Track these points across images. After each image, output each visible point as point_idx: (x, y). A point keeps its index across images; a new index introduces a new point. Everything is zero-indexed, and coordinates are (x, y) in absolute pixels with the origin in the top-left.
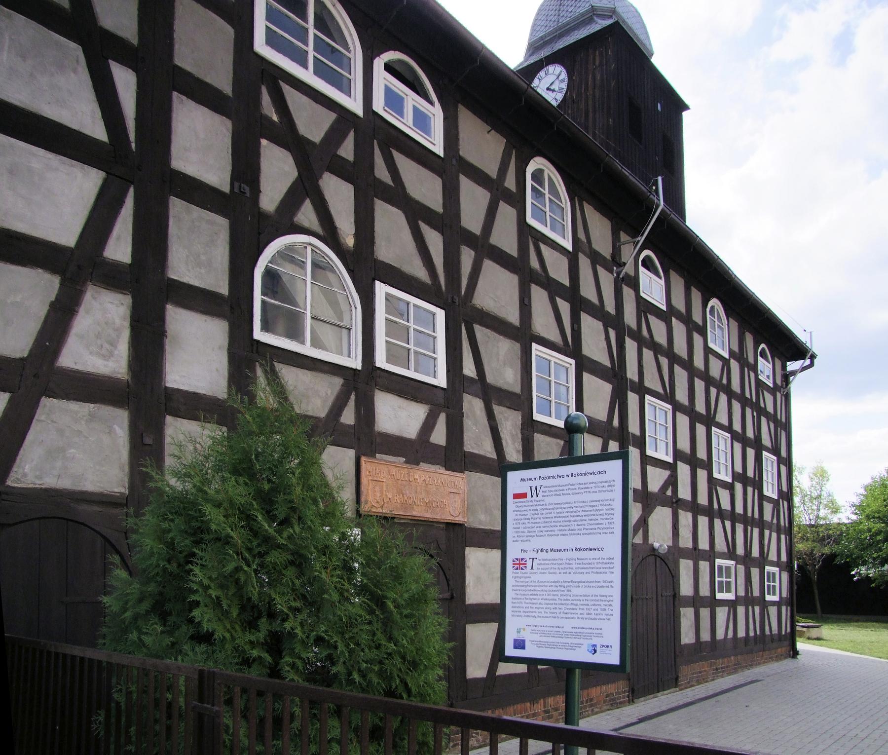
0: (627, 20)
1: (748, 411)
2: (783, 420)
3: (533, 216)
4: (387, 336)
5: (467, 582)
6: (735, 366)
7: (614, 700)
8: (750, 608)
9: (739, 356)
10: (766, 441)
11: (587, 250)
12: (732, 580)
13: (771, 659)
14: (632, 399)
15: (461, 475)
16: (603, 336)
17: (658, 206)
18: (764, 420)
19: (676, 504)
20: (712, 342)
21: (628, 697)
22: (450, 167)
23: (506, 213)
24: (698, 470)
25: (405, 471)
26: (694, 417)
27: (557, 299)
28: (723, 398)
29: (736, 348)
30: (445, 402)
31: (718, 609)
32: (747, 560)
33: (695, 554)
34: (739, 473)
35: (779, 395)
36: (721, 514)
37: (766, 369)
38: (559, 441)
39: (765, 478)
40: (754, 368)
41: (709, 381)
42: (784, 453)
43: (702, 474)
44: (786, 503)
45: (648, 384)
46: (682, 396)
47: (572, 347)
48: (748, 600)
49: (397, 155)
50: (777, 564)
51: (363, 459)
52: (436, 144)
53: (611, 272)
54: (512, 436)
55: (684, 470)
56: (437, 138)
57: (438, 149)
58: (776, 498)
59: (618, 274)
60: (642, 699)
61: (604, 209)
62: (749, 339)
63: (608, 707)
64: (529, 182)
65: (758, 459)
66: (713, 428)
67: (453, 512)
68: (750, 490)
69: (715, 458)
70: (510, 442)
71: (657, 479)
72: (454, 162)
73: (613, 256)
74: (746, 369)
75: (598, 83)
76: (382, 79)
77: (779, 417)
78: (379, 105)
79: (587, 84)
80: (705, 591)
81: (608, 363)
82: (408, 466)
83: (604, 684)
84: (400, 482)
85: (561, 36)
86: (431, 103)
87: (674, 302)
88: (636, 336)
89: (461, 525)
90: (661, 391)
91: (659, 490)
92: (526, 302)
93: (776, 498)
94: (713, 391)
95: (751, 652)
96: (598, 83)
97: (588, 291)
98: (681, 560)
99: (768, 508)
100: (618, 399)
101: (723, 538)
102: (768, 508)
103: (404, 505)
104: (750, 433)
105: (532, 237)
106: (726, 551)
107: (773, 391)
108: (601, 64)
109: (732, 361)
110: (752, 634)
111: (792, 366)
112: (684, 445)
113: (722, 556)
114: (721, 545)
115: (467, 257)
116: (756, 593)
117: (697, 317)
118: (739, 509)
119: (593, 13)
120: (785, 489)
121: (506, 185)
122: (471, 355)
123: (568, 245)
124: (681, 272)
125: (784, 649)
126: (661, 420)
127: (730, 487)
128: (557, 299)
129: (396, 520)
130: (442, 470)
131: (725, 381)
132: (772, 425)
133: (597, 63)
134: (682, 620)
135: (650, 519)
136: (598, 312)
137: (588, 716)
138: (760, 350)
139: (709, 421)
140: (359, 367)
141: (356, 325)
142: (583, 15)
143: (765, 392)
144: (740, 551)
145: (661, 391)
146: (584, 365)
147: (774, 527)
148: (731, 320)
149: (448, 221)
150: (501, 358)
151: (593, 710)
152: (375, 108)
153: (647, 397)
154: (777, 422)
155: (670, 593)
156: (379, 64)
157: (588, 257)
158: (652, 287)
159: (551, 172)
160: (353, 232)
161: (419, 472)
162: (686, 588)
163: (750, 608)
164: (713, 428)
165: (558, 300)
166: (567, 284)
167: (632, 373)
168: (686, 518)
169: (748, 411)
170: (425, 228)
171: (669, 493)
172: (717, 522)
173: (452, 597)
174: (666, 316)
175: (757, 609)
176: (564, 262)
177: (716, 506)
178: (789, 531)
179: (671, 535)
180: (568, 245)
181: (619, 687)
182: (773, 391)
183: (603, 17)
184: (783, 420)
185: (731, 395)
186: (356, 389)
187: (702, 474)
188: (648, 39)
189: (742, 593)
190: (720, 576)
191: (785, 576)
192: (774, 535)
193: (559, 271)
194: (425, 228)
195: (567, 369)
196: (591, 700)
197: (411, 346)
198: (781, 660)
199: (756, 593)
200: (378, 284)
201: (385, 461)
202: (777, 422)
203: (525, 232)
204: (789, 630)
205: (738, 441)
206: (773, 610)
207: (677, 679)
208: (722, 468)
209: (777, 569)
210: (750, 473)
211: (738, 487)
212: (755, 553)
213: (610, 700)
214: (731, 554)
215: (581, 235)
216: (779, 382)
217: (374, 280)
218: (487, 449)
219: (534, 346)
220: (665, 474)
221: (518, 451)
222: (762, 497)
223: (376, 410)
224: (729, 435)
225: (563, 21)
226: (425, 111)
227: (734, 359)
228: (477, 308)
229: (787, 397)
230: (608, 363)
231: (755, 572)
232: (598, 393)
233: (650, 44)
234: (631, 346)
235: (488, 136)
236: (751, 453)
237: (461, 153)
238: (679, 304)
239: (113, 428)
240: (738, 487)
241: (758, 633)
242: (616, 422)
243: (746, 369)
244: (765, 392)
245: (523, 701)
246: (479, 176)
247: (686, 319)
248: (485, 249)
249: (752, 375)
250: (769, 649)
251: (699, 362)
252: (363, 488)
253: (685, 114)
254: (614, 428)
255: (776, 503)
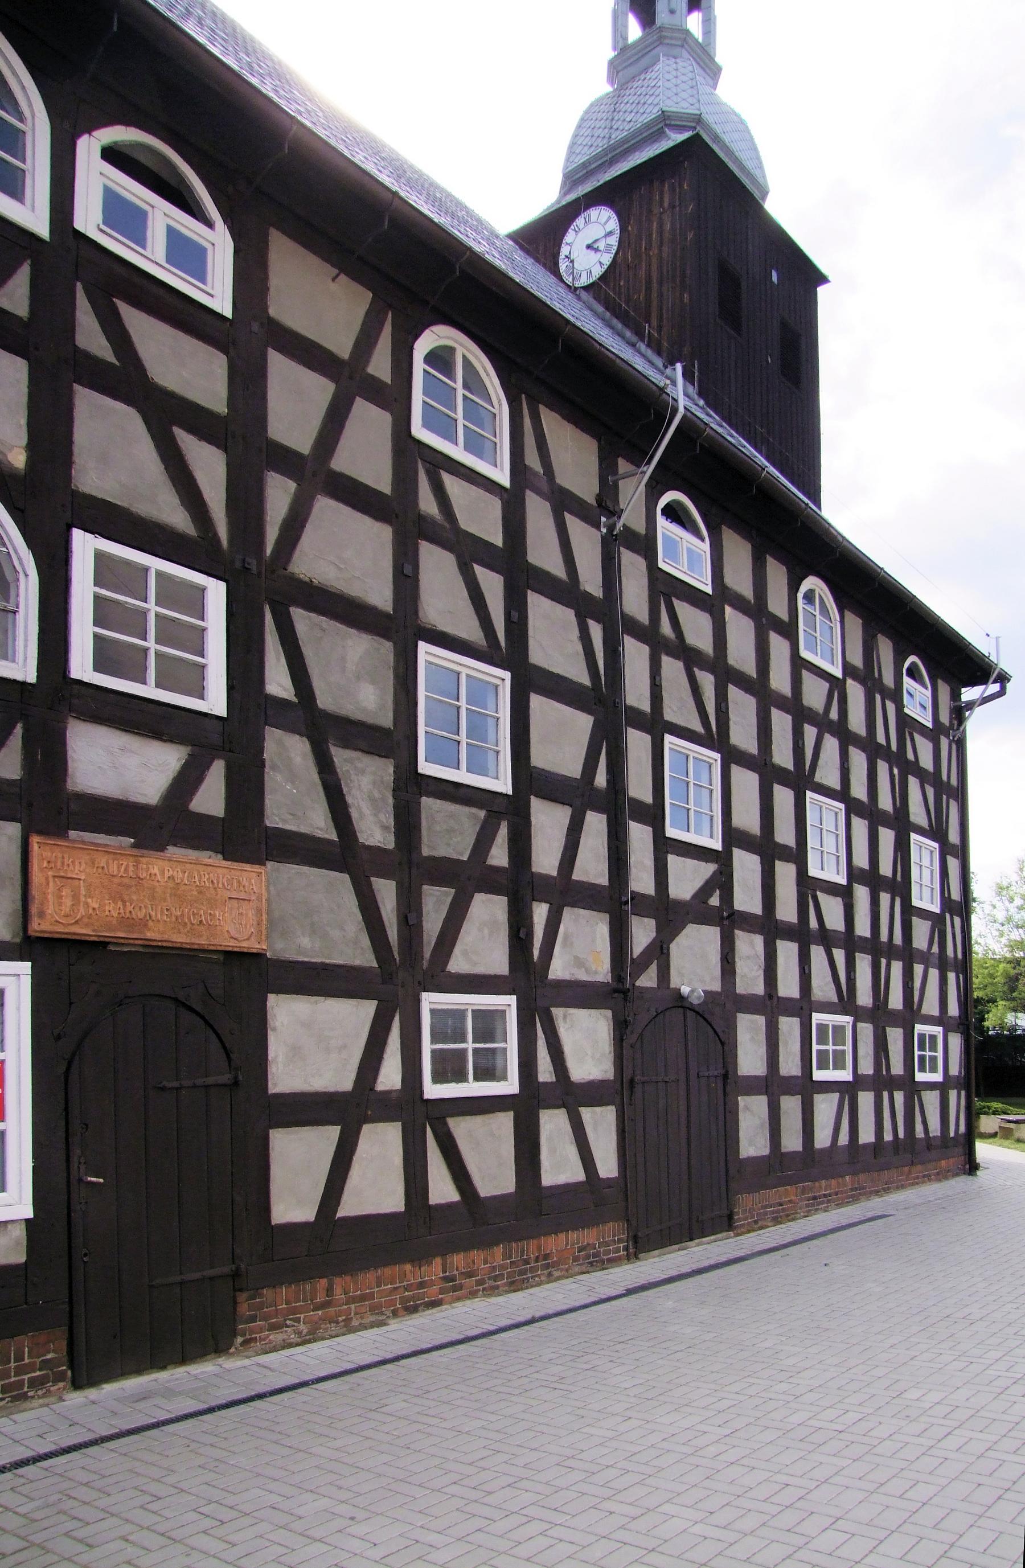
0: (722, 136)
1: (882, 767)
2: (954, 781)
3: (426, 424)
4: (94, 625)
5: (271, 1055)
6: (855, 692)
7: (595, 1255)
8: (885, 1094)
9: (866, 675)
10: (917, 814)
11: (545, 487)
12: (848, 1048)
13: (927, 1178)
14: (637, 743)
15: (257, 868)
16: (575, 633)
17: (675, 410)
18: (913, 784)
19: (729, 921)
20: (806, 648)
21: (626, 1249)
22: (248, 338)
23: (368, 422)
24: (777, 862)
25: (128, 863)
26: (769, 775)
27: (476, 567)
28: (831, 745)
29: (857, 660)
30: (230, 745)
31: (818, 1098)
32: (879, 1015)
33: (770, 1005)
34: (862, 870)
35: (944, 742)
36: (826, 938)
37: (918, 700)
38: (474, 810)
39: (810, 844)
40: (896, 695)
41: (801, 715)
42: (954, 837)
43: (785, 873)
44: (957, 921)
45: (670, 715)
46: (743, 735)
47: (509, 650)
48: (881, 1082)
49: (124, 309)
50: (941, 1020)
51: (35, 840)
52: (218, 294)
53: (597, 526)
54: (372, 800)
55: (746, 866)
56: (218, 284)
57: (222, 303)
58: (937, 911)
59: (611, 528)
60: (656, 1252)
61: (581, 417)
62: (885, 649)
63: (584, 1268)
64: (419, 366)
65: (902, 848)
66: (809, 794)
67: (235, 929)
68: (885, 898)
69: (812, 841)
70: (367, 811)
71: (686, 879)
72: (255, 327)
73: (599, 499)
74: (878, 697)
75: (667, 235)
76: (94, 177)
77: (945, 778)
78: (88, 218)
79: (650, 241)
80: (790, 1065)
81: (585, 680)
82: (135, 852)
83: (573, 1230)
84: (116, 880)
85: (612, 162)
86: (210, 224)
87: (729, 580)
88: (648, 634)
89: (257, 957)
90: (699, 728)
91: (695, 896)
92: (408, 570)
93: (937, 911)
94: (810, 733)
95: (887, 1167)
96: (667, 235)
97: (543, 552)
98: (740, 1016)
99: (921, 931)
100: (608, 740)
101: (830, 979)
102: (921, 931)
103: (127, 922)
104: (885, 802)
105: (424, 461)
106: (835, 999)
107: (934, 734)
108: (672, 206)
109: (850, 682)
110: (888, 1137)
111: (969, 694)
112: (747, 817)
113: (826, 1008)
114: (823, 988)
115: (279, 494)
116: (897, 1068)
117: (777, 606)
118: (863, 928)
119: (665, 121)
120: (956, 895)
121: (370, 370)
122: (283, 660)
123: (503, 477)
124: (744, 529)
125: (957, 1160)
126: (829, 824)
127: (845, 893)
128: (476, 567)
129: (112, 948)
130: (217, 859)
131: (834, 715)
132: (930, 791)
133: (666, 205)
134: (742, 1116)
135: (673, 947)
136: (565, 591)
137: (539, 1285)
138: (906, 665)
139: (801, 780)
140: (32, 677)
141: (27, 606)
142: (648, 126)
143: (916, 736)
144: (864, 997)
145: (699, 728)
146: (529, 681)
147: (935, 960)
148: (848, 614)
149: (241, 430)
150: (350, 666)
151: (550, 1274)
152: (79, 225)
153: (668, 738)
154: (942, 788)
155: (717, 1071)
156: (88, 149)
157: (547, 499)
158: (686, 553)
159: (466, 349)
160: (24, 441)
161: (160, 863)
162: (750, 1060)
163: (885, 1094)
164: (809, 794)
165: (478, 569)
166: (499, 541)
167: (636, 694)
168: (749, 947)
169: (882, 767)
170: (188, 443)
171: (715, 901)
172: (817, 953)
173: (236, 1083)
174: (715, 603)
175: (899, 1097)
176: (494, 507)
177: (813, 924)
178: (964, 965)
179: (718, 972)
180: (503, 477)
181: (610, 1233)
182: (934, 734)
183: (681, 128)
184: (954, 781)
185: (846, 739)
186: (24, 717)
187: (785, 873)
188: (761, 167)
189: (867, 1068)
190: (822, 1040)
191: (956, 1041)
192: (934, 974)
193: (482, 518)
194: (188, 443)
195: (497, 686)
196: (546, 1257)
197: (151, 644)
198: (946, 1178)
199: (897, 1068)
200: (78, 536)
201: (83, 842)
202: (942, 788)
203: (407, 451)
204: (962, 1129)
205: (861, 816)
206: (931, 1100)
207: (730, 1217)
208: (926, 893)
209: (940, 1029)
210: (886, 868)
211: (862, 894)
212: (896, 1001)
213: (588, 1257)
214: (846, 1003)
215: (532, 460)
216: (945, 718)
217: (69, 528)
218: (318, 823)
219: (423, 647)
220: (708, 869)
221: (385, 828)
222: (909, 911)
223: (70, 753)
224: (842, 806)
225: (618, 136)
226: (195, 238)
227: (854, 679)
228: (300, 581)
229: (960, 745)
230: (585, 680)
231: (895, 1036)
232: (563, 739)
233: (764, 177)
234: (635, 654)
235: (333, 287)
236: (887, 837)
237: (272, 312)
238: (740, 578)
239: (336, 1075)
240: (862, 894)
241: (901, 1134)
242: (601, 779)
243: (878, 697)
244: (916, 736)
245: (402, 1261)
246: (310, 354)
247: (756, 610)
248: (318, 475)
249: (891, 707)
250: (922, 1163)
251: (780, 681)
252: (35, 892)
253: (822, 291)
254: (598, 790)
255: (937, 921)
